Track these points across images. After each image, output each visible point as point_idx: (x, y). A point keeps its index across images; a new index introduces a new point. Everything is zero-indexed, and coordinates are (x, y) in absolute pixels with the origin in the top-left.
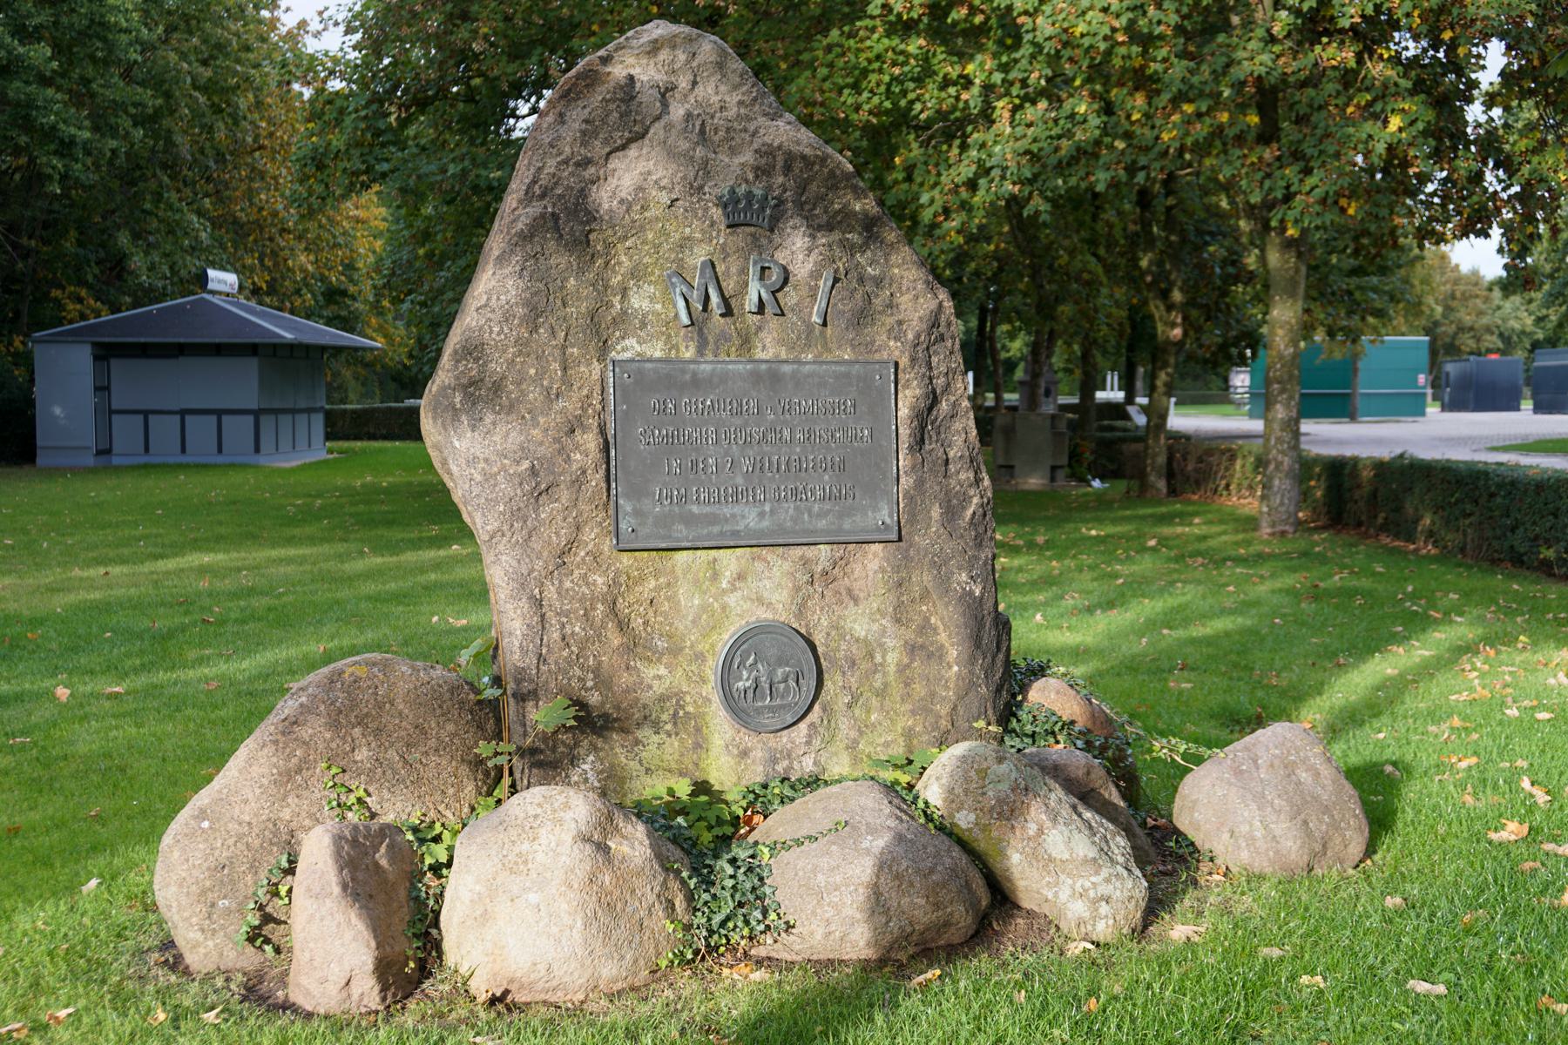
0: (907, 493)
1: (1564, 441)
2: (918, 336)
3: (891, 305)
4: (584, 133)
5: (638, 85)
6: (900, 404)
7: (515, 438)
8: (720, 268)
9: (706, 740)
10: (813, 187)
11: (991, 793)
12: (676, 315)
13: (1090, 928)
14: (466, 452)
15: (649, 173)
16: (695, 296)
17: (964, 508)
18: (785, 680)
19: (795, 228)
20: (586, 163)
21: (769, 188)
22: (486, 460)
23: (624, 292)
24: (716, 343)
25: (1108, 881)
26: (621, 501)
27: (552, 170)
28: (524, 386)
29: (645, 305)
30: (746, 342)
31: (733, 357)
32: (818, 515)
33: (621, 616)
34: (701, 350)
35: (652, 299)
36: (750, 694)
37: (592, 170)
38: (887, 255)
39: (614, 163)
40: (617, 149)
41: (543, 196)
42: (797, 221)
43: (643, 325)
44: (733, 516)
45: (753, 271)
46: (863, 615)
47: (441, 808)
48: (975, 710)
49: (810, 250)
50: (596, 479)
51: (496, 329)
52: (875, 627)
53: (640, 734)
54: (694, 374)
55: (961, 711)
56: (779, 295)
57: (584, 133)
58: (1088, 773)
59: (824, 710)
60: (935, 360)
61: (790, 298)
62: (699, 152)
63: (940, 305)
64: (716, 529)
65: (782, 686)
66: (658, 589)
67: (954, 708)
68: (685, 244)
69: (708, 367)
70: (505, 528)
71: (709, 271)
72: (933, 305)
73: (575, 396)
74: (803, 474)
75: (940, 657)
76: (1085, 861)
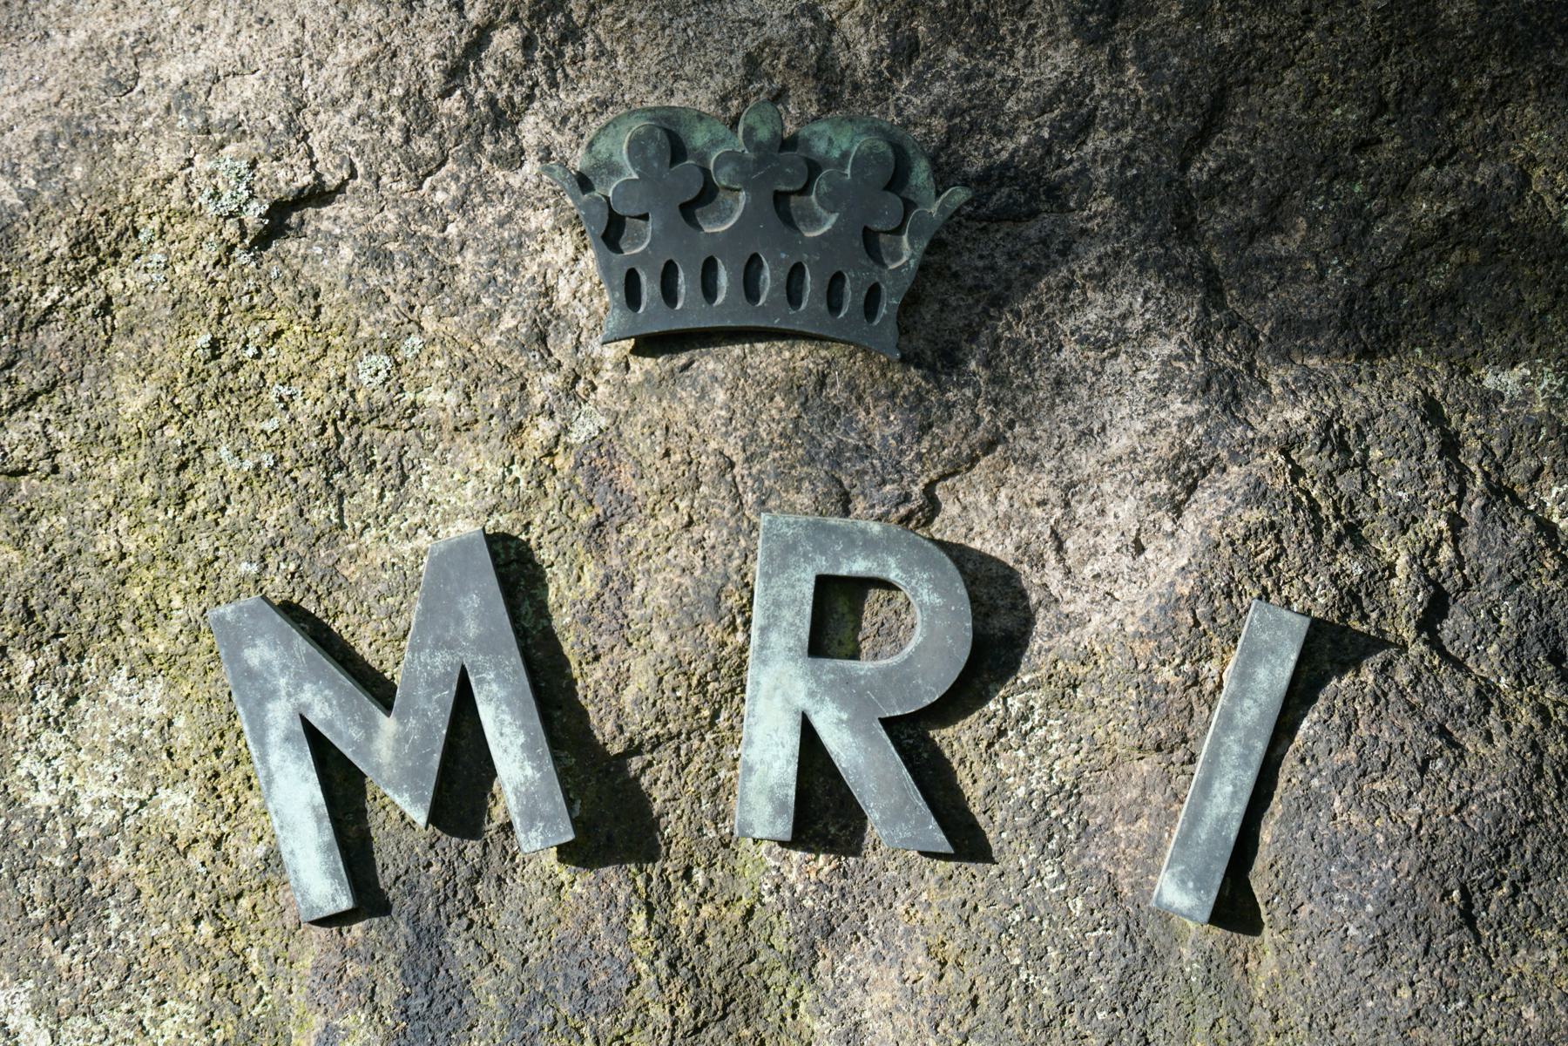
8: (568, 593)
12: (273, 861)
45: (784, 605)
56: (958, 740)
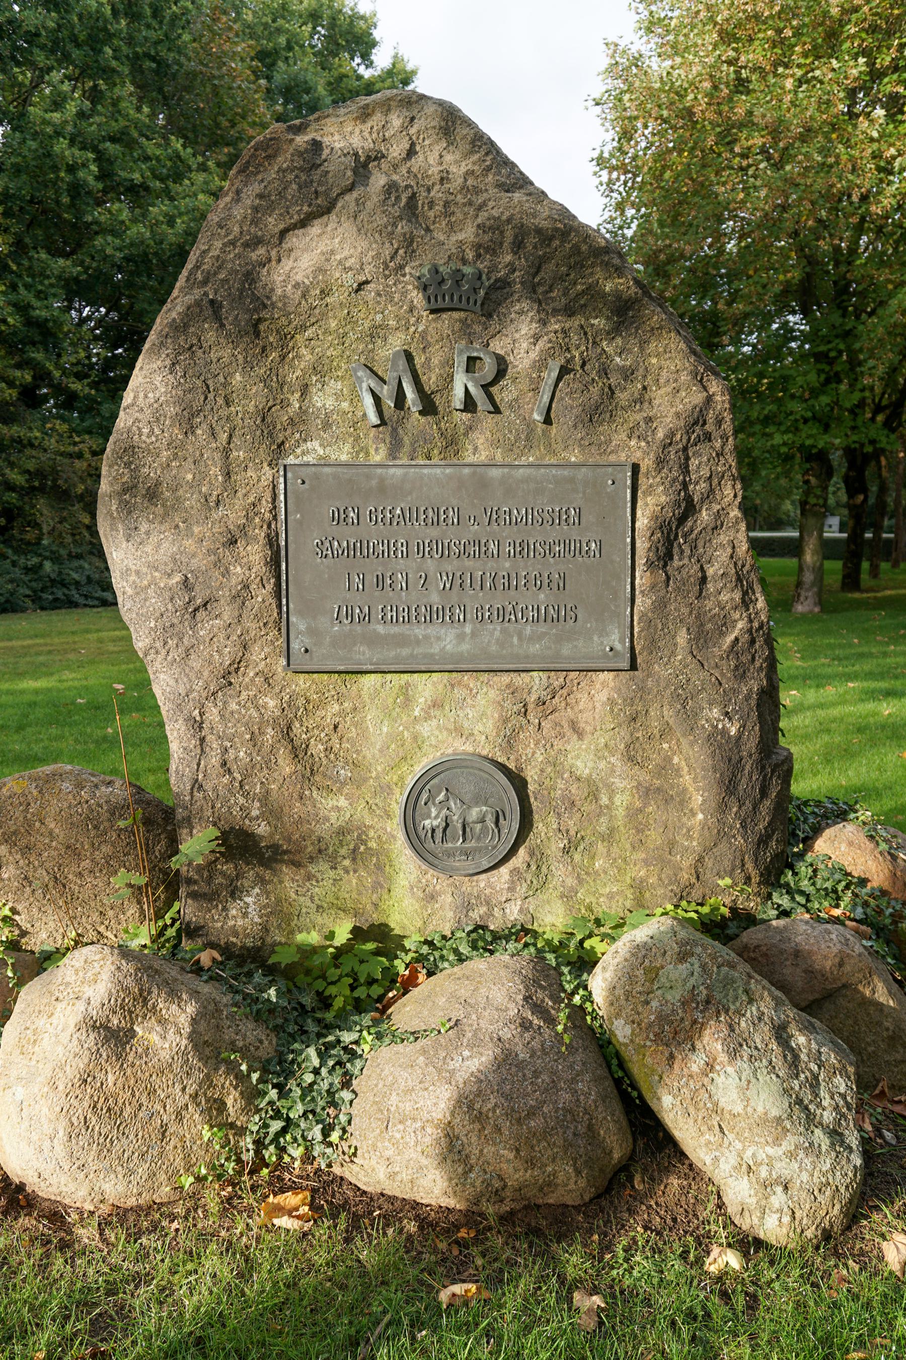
0: (643, 615)
1: (4, 611)
2: (672, 434)
3: (641, 399)
4: (256, 209)
5: (326, 152)
6: (639, 513)
7: (168, 548)
8: (419, 361)
9: (389, 879)
10: (551, 266)
11: (654, 1004)
12: (365, 415)
13: (756, 1221)
14: (134, 558)
15: (332, 252)
16: (387, 393)
17: (722, 634)
18: (482, 821)
19: (521, 313)
20: (256, 242)
21: (493, 269)
22: (138, 573)
23: (305, 390)
24: (412, 445)
25: (791, 1155)
26: (293, 619)
27: (217, 253)
28: (181, 492)
29: (330, 403)
30: (452, 444)
31: (435, 461)
32: (531, 639)
33: (297, 743)
34: (393, 453)
35: (338, 396)
36: (439, 834)
37: (261, 251)
38: (643, 344)
39: (294, 240)
40: (294, 227)
41: (205, 282)
42: (525, 305)
43: (327, 425)
44: (426, 637)
45: (460, 362)
46: (587, 747)
47: (102, 929)
48: (727, 864)
49: (536, 338)
50: (263, 595)
51: (145, 431)
52: (602, 765)
53: (312, 869)
54: (382, 480)
55: (709, 862)
56: (494, 390)
57: (256, 209)
58: (841, 964)
59: (532, 854)
60: (694, 463)
61: (505, 393)
62: (402, 227)
63: (709, 399)
64: (405, 652)
65: (479, 826)
66: (342, 714)
67: (700, 860)
68: (376, 333)
69: (399, 472)
70: (158, 644)
71: (402, 363)
72: (698, 398)
73: (239, 503)
74: (512, 592)
75: (682, 802)
76: (764, 1121)
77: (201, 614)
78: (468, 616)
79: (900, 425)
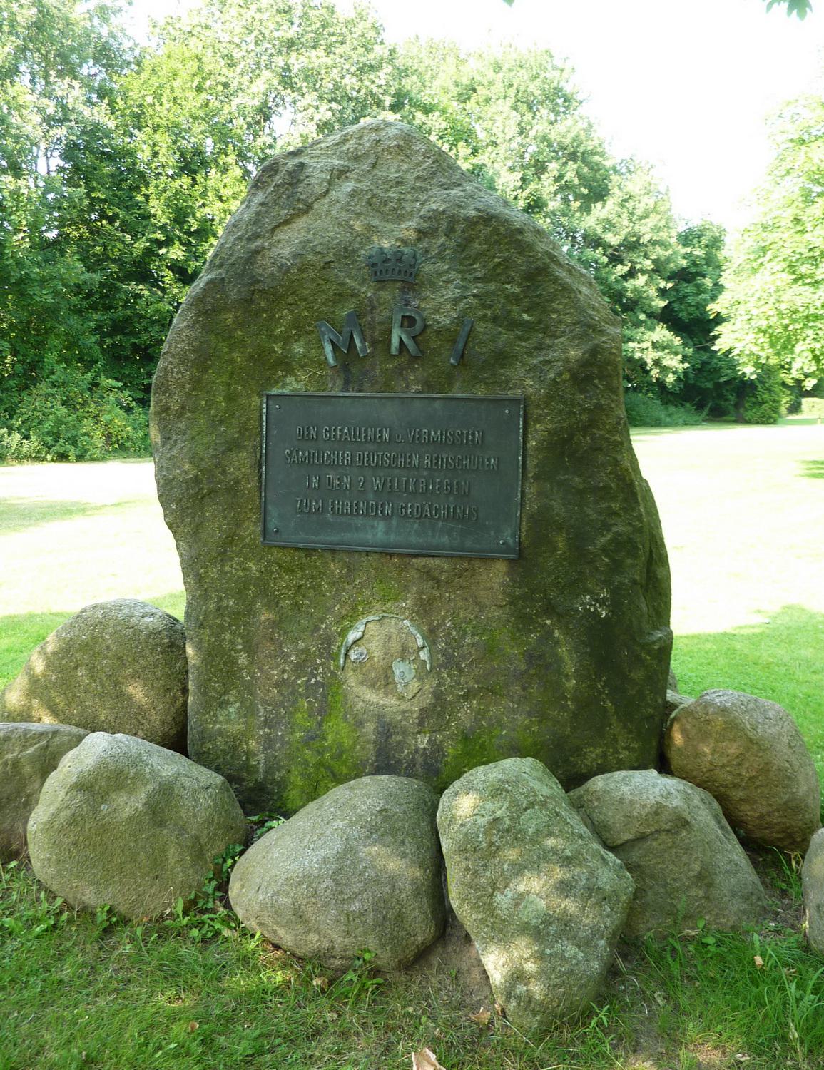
20: (256, 236)
77: (207, 500)
78: (395, 512)
79: (812, 1068)
